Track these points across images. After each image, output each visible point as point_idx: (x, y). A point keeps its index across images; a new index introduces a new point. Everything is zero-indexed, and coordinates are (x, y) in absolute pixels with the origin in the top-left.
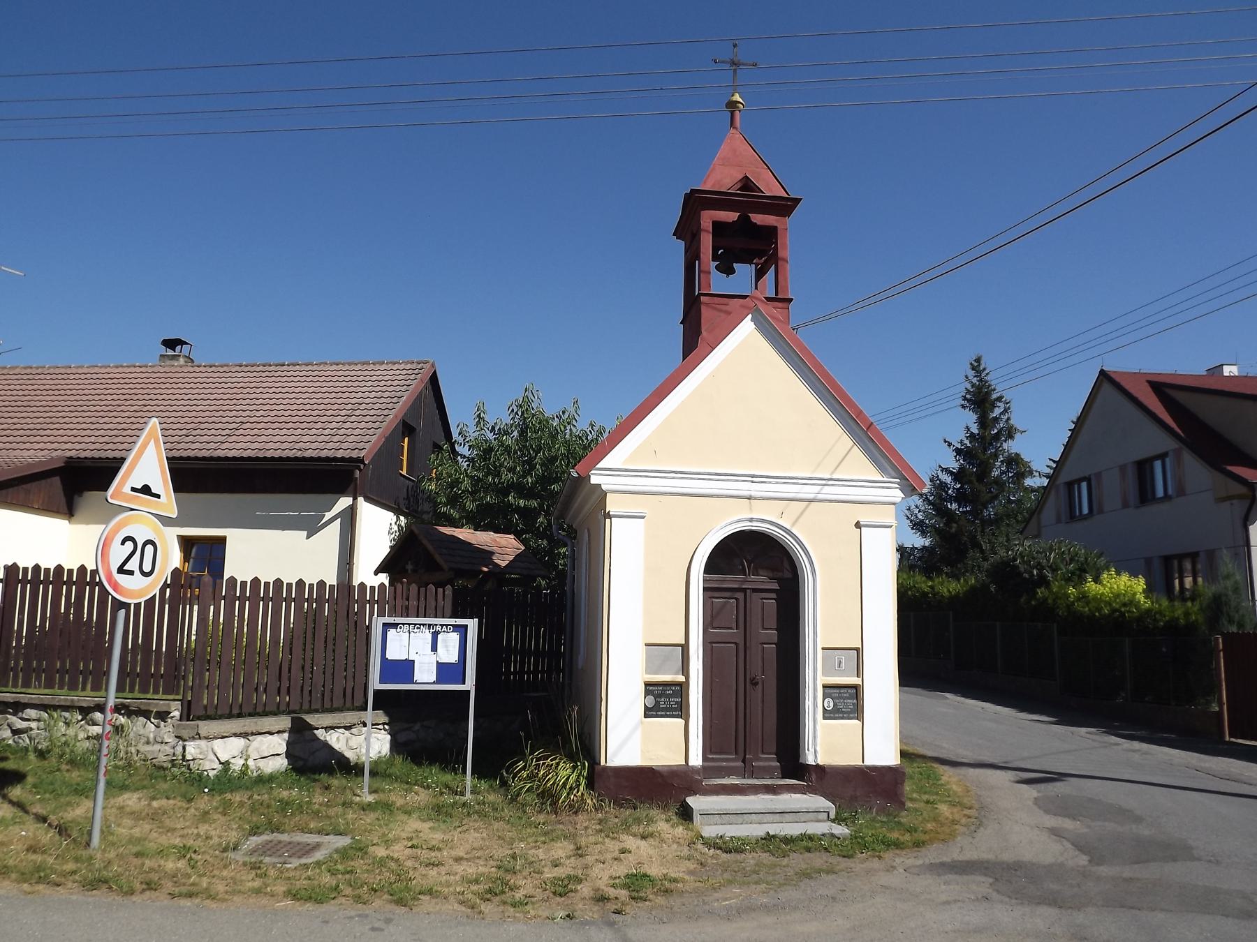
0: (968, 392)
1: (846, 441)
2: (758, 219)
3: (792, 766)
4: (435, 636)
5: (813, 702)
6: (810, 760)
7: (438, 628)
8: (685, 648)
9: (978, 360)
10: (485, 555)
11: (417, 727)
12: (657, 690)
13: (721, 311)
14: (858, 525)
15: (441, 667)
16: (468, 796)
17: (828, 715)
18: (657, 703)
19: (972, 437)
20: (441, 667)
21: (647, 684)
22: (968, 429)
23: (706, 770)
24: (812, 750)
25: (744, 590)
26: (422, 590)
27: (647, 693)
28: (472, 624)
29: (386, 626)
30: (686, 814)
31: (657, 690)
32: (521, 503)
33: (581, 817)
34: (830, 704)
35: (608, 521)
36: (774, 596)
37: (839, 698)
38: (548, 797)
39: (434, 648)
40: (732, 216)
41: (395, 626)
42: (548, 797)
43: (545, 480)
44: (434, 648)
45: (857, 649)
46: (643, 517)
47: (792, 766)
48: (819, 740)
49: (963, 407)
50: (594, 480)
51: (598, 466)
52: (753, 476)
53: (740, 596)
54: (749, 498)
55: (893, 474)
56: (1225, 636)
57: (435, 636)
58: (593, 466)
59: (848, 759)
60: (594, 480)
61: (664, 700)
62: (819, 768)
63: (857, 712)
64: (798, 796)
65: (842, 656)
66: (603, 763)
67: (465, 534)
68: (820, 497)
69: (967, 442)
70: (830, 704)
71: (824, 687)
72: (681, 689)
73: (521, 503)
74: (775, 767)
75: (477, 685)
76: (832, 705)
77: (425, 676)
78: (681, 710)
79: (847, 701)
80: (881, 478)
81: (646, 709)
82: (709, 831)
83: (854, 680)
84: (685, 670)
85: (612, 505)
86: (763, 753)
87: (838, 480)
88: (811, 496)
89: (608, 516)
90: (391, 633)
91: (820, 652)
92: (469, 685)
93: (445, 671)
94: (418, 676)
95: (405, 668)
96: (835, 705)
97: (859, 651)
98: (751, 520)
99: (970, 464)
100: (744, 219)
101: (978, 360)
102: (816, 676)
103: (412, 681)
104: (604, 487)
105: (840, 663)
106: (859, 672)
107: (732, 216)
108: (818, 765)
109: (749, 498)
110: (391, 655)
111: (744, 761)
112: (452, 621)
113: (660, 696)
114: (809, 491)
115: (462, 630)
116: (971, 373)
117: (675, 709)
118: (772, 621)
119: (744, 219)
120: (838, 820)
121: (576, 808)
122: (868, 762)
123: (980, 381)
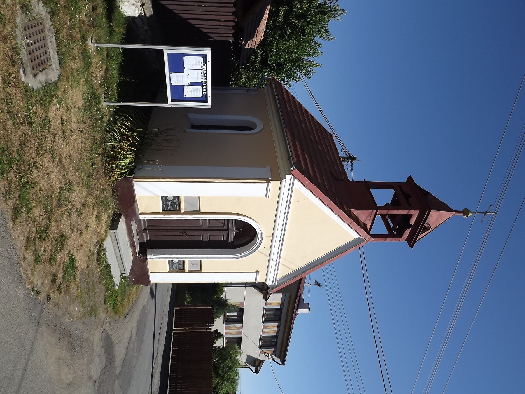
1: (295, 268)
2: (408, 232)
3: (143, 249)
4: (201, 84)
5: (176, 257)
6: (148, 257)
7: (205, 87)
8: (198, 212)
10: (251, 36)
11: (146, 27)
12: (176, 201)
13: (367, 218)
14: (257, 272)
15: (182, 87)
16: (105, 104)
18: (169, 201)
20: (182, 87)
21: (179, 197)
23: (139, 222)
24: (153, 257)
25: (228, 229)
26: (232, 5)
27: (174, 197)
28: (209, 104)
29: (205, 57)
30: (114, 224)
31: (176, 201)
32: (282, 13)
33: (104, 178)
35: (265, 181)
36: (225, 239)
37: (179, 265)
38: (112, 157)
39: (192, 84)
40: (412, 221)
41: (205, 61)
42: (112, 157)
43: (292, 26)
44: (192, 84)
45: (201, 270)
46: (266, 196)
47: (143, 249)
50: (288, 177)
51: (296, 180)
52: (283, 239)
53: (225, 228)
54: (273, 237)
55: (279, 283)
56: (213, 308)
57: (201, 84)
58: (295, 177)
60: (288, 177)
61: (171, 204)
62: (145, 260)
64: (131, 254)
66: (134, 180)
67: (265, 18)
68: (271, 261)
71: (183, 261)
72: (177, 210)
73: (282, 13)
75: (171, 108)
77: (173, 79)
78: (166, 210)
80: (278, 278)
81: (166, 197)
82: (108, 244)
83: (187, 269)
84: (187, 213)
85: (275, 184)
86: (150, 235)
87: (278, 266)
88: (271, 257)
89: (268, 182)
90: (201, 59)
92: (171, 103)
93: (178, 91)
94: (174, 75)
95: (178, 65)
98: (262, 237)
100: (410, 226)
103: (171, 71)
104: (284, 181)
107: (412, 221)
108: (146, 259)
109: (273, 237)
110: (186, 58)
111: (145, 229)
112: (209, 94)
113: (173, 202)
114: (274, 257)
115: (204, 99)
117: (167, 208)
118: (213, 238)
119: (410, 226)
120: (122, 277)
121: (108, 172)
122: (151, 275)
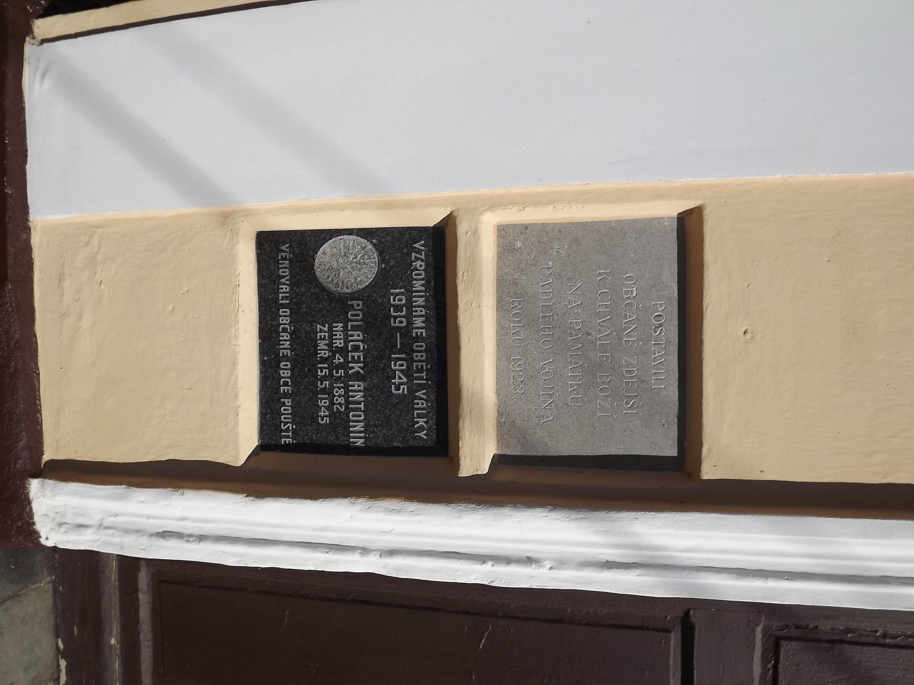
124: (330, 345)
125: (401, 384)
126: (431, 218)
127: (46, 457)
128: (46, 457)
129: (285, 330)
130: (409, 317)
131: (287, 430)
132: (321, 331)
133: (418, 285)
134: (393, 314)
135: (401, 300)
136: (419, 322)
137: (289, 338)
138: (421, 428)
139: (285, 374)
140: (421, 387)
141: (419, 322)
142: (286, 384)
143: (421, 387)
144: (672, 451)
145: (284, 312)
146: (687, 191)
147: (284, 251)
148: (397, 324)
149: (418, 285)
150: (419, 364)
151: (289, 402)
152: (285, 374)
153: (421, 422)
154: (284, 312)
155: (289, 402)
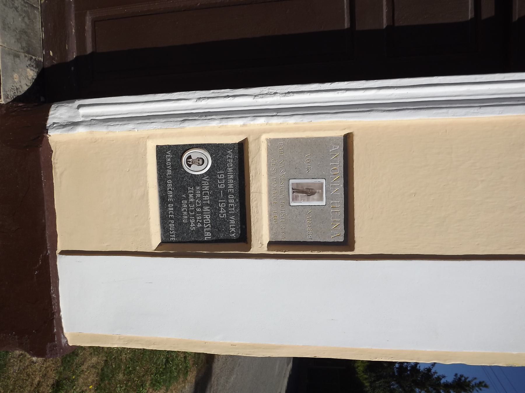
0: (466, 379)
9: (486, 386)
17: (170, 158)
19: (439, 379)
22: (444, 377)
34: (200, 167)
37: (215, 193)
45: (348, 242)
48: (101, 132)
49: (456, 375)
59: (72, 216)
63: (180, 241)
65: (325, 200)
69: (436, 376)
70: (200, 167)
71: (241, 149)
74: (344, 26)
76: (196, 170)
79: (205, 211)
83: (262, 233)
91: (332, 127)
96: (196, 180)
97: (343, 246)
99: (422, 376)
101: (486, 386)
102: (265, 119)
105: (309, 192)
106: (284, 248)
116: (477, 381)
122: (64, 264)
123: (473, 386)
124: (194, 196)
125: (224, 213)
126: (236, 140)
127: (516, 17)
128: (516, 17)
129: (170, 190)
130: (226, 184)
131: (173, 234)
132: (190, 190)
133: (230, 170)
134: (219, 182)
135: (222, 176)
136: (231, 186)
137: (208, 184)
138: (233, 232)
139: (170, 185)
140: (232, 215)
141: (231, 186)
142: (171, 214)
143: (232, 215)
144: (341, 239)
145: (169, 182)
146: (349, 127)
147: (168, 154)
148: (221, 187)
149: (230, 170)
150: (232, 205)
151: (173, 221)
152: (170, 185)
153: (233, 229)
154: (169, 182)
155: (173, 221)
